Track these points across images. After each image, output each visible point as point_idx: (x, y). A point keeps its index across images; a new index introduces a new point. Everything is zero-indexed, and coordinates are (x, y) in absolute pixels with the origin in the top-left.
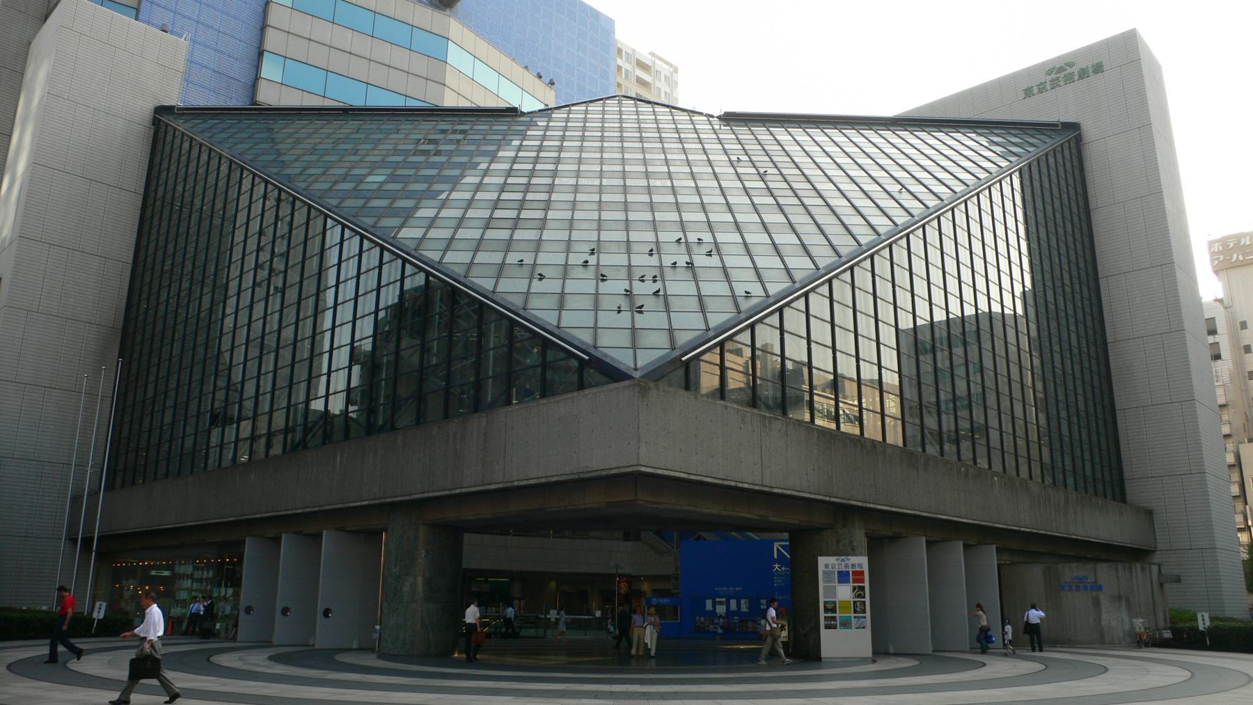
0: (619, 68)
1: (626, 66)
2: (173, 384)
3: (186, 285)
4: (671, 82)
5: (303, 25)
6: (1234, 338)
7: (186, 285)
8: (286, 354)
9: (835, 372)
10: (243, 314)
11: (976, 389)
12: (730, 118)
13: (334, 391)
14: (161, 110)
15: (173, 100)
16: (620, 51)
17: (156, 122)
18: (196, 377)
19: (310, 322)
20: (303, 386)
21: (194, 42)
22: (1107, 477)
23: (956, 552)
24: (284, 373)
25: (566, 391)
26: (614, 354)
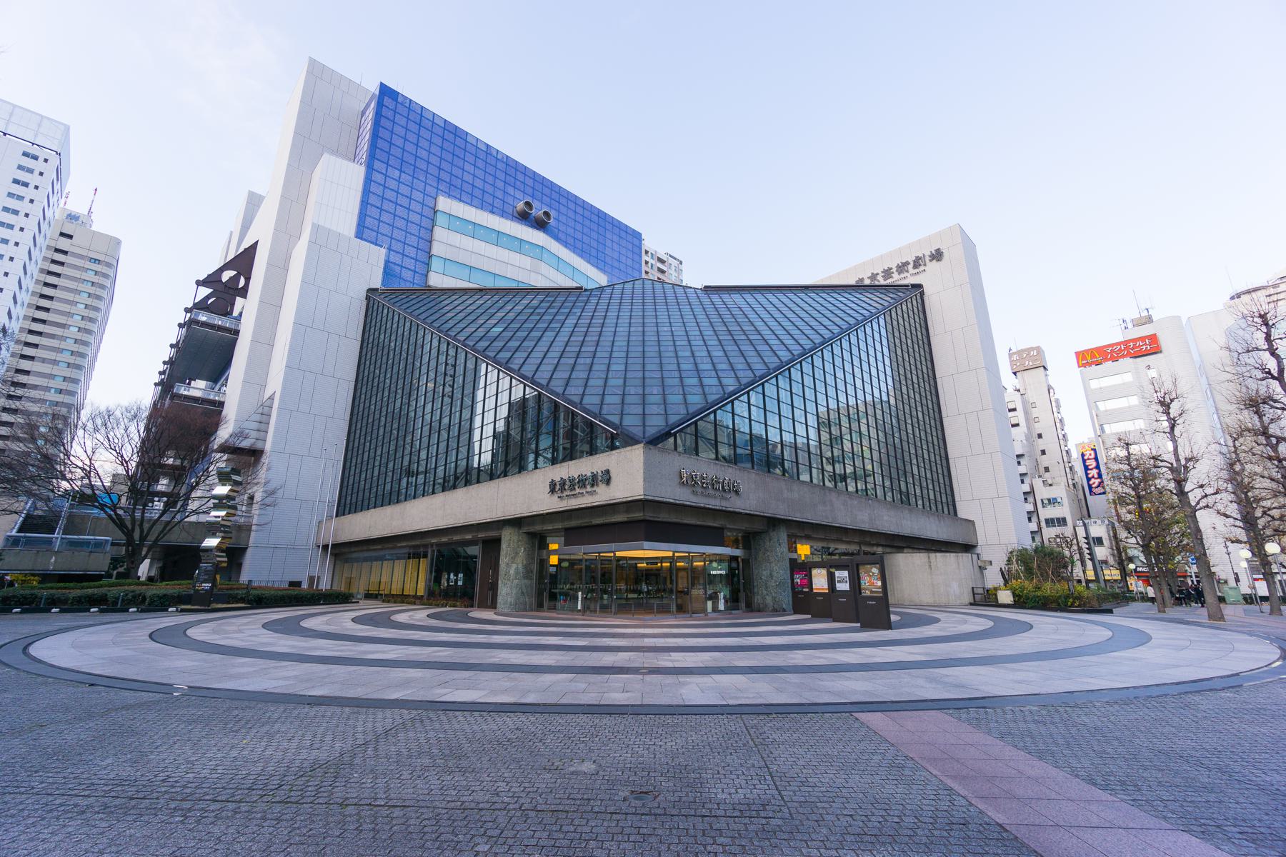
0: (647, 263)
1: (651, 261)
2: (379, 452)
3: (386, 394)
4: (679, 271)
5: (457, 239)
6: (1026, 413)
7: (386, 394)
8: (444, 434)
9: (751, 434)
10: (425, 410)
11: (857, 448)
12: (707, 289)
13: (484, 453)
14: (371, 290)
15: (377, 284)
16: (647, 252)
17: (368, 298)
18: (392, 447)
19: (458, 414)
20: (454, 452)
21: (390, 249)
22: (944, 500)
23: (807, 344)
24: (443, 445)
25: (603, 452)
26: (631, 429)
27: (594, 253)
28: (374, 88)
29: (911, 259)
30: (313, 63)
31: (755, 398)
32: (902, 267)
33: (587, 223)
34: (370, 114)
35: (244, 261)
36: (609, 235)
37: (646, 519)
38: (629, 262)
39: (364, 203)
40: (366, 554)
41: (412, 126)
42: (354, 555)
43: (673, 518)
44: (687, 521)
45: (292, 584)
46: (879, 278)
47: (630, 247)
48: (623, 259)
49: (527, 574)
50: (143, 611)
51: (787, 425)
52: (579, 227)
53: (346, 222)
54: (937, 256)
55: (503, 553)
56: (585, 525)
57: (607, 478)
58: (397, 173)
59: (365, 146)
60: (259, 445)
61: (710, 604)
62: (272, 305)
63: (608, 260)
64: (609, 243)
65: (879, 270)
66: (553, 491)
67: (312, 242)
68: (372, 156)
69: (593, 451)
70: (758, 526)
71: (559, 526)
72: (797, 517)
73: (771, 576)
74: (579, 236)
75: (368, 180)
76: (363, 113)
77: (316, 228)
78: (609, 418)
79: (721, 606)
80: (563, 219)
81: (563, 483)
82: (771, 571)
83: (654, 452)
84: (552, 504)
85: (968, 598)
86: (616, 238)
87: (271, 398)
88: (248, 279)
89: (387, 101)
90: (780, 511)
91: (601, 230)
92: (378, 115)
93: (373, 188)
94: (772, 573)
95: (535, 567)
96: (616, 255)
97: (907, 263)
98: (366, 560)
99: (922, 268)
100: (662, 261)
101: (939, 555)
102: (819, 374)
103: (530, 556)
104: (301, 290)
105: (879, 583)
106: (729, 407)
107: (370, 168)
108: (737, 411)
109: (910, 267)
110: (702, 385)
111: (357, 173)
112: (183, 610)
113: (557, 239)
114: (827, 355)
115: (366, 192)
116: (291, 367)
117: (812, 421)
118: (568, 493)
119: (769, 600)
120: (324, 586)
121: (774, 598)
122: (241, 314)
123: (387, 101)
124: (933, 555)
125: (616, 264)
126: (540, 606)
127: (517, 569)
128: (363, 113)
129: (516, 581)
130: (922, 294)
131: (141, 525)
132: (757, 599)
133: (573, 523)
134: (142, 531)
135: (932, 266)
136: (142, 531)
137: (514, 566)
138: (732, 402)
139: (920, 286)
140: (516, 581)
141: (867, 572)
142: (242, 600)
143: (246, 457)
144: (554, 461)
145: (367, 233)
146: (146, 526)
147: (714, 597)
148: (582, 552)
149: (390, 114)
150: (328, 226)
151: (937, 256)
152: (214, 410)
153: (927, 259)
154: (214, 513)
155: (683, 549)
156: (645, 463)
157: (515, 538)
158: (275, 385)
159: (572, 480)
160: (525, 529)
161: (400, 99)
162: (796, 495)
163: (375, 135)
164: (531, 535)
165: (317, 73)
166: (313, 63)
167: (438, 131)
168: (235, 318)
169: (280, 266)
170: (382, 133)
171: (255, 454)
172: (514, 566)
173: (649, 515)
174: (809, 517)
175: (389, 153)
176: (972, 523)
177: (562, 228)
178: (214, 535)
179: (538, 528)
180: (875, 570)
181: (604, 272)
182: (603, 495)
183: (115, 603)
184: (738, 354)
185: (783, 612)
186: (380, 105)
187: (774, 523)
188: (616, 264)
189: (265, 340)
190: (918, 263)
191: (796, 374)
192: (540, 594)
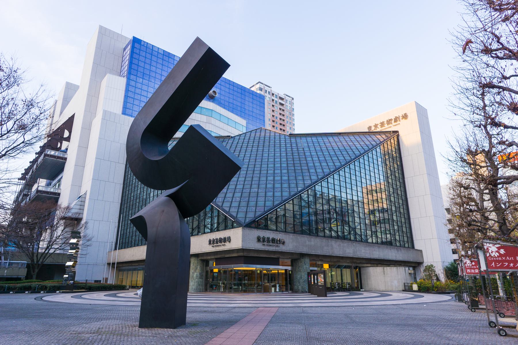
1: (275, 99)
27: (239, 108)
28: (131, 38)
29: (393, 118)
30: (101, 27)
31: (336, 176)
32: (389, 122)
33: (235, 93)
34: (128, 51)
35: (69, 124)
36: (247, 98)
37: (245, 256)
38: (258, 112)
39: (126, 97)
40: (130, 267)
41: (149, 56)
42: (124, 268)
43: (256, 255)
44: (265, 256)
45: (96, 281)
46: (379, 126)
47: (258, 103)
48: (255, 110)
49: (201, 277)
50: (31, 293)
51: (354, 193)
52: (231, 96)
53: (117, 107)
54: (405, 116)
55: (191, 268)
56: (223, 258)
57: (229, 239)
58: (141, 80)
59: (126, 68)
60: (80, 216)
61: (273, 289)
62: (84, 147)
63: (247, 112)
64: (247, 103)
65: (378, 122)
66: (210, 243)
67: (103, 119)
68: (129, 73)
69: (226, 228)
70: (295, 257)
71: (213, 257)
72: (313, 252)
73: (301, 278)
74: (231, 101)
75: (128, 85)
76: (125, 49)
77: (105, 112)
78: (232, 213)
79: (278, 290)
80: (223, 93)
81: (214, 240)
82: (301, 275)
83: (248, 231)
84: (210, 249)
85: (402, 288)
86: (251, 100)
87: (85, 194)
88: (70, 132)
89: (136, 45)
90: (305, 250)
91: (243, 96)
92: (132, 52)
93: (131, 89)
94: (301, 276)
95: (204, 274)
96: (251, 109)
97: (391, 120)
98: (130, 270)
99: (398, 122)
100: (281, 99)
101: (388, 268)
102: (371, 160)
103: (202, 269)
104: (99, 142)
105: (323, 280)
106: (320, 184)
107: (128, 79)
108: (329, 181)
109: (393, 121)
110: (313, 160)
111: (123, 81)
112: (63, 292)
113: (220, 104)
114: (374, 152)
115: (127, 90)
116: (95, 179)
117: (365, 191)
118: (216, 245)
119: (300, 287)
120: (110, 282)
121: (302, 287)
122: (67, 149)
123: (136, 45)
124: (385, 268)
125: (251, 113)
126: (206, 290)
127: (197, 275)
128: (125, 49)
129: (196, 280)
130: (398, 136)
131: (37, 256)
132: (296, 287)
133: (219, 256)
134: (37, 258)
135: (403, 122)
136: (37, 258)
137: (196, 273)
138: (315, 186)
139: (397, 132)
140: (196, 280)
141: (320, 276)
142: (83, 288)
143: (74, 222)
144: (212, 231)
145: (128, 111)
146: (39, 256)
147: (275, 286)
148: (223, 267)
149: (138, 51)
150: (109, 110)
151: (405, 116)
152: (56, 197)
153: (401, 118)
154: (70, 251)
155: (259, 267)
156: (242, 235)
157: (196, 262)
158: (86, 187)
159: (217, 239)
160: (200, 258)
161: (142, 43)
162: (313, 243)
163: (131, 63)
164: (203, 261)
165: (103, 32)
166: (101, 27)
167: (160, 56)
168: (63, 151)
169: (87, 129)
170: (135, 61)
171: (78, 220)
172: (196, 273)
173: (245, 254)
174: (319, 252)
175: (137, 71)
176: (421, 251)
177: (222, 98)
178: (70, 261)
179: (205, 258)
180: (322, 276)
181: (244, 118)
182: (228, 246)
183: (35, 289)
184: (324, 151)
185: (306, 292)
186: (133, 47)
187: (303, 255)
188: (251, 113)
189: (80, 166)
190: (396, 119)
191: (361, 160)
192: (206, 285)
